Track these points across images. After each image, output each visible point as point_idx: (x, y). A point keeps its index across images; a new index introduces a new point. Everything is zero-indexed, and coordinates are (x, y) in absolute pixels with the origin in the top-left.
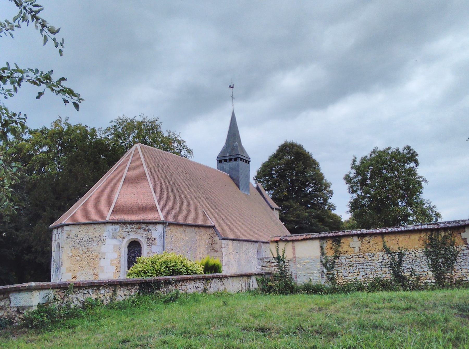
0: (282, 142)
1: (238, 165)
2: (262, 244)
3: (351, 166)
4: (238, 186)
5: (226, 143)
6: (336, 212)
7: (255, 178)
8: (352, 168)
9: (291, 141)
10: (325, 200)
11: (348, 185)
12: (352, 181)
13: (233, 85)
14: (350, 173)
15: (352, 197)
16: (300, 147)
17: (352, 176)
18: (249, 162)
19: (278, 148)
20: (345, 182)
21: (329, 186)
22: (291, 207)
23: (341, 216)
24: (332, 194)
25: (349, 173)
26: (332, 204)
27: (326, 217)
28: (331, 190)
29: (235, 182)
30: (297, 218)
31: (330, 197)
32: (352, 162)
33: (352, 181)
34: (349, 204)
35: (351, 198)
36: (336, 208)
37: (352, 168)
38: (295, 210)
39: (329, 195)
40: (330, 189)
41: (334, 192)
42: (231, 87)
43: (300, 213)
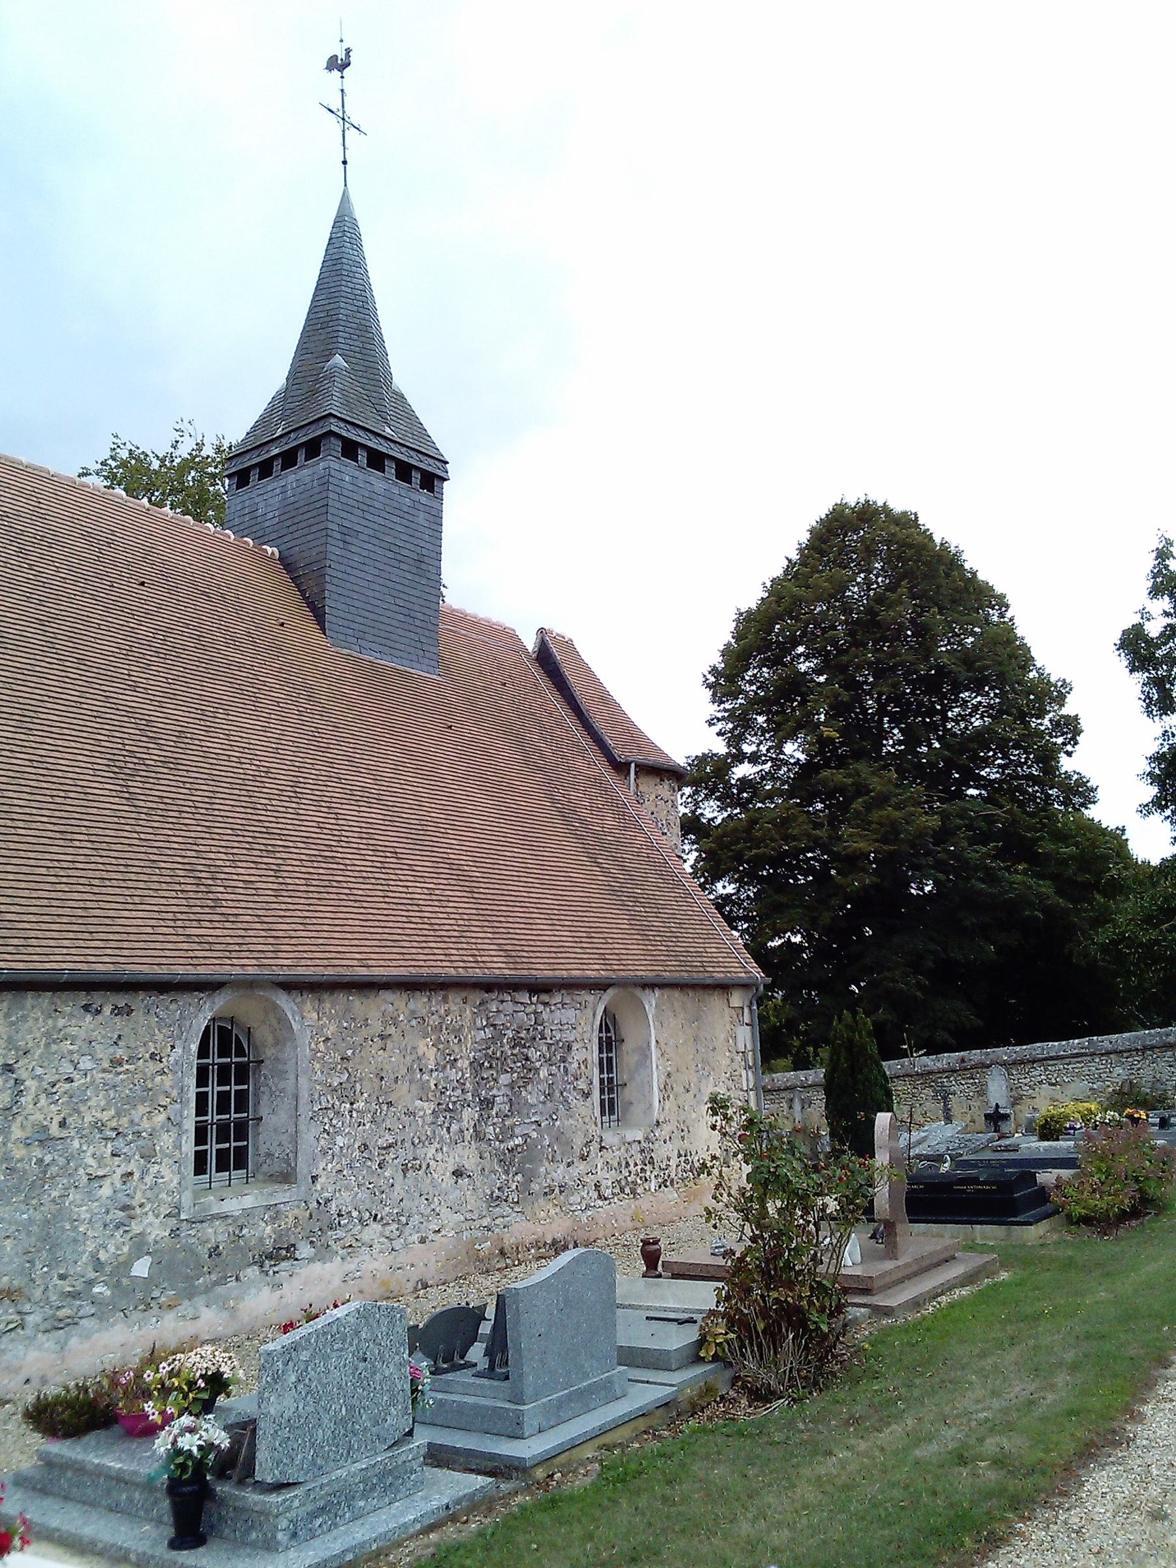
0: (821, 510)
1: (325, 482)
2: (283, 1001)
3: (1150, 584)
4: (319, 617)
5: (294, 376)
6: (1103, 813)
7: (712, 679)
8: (1156, 592)
9: (862, 501)
10: (1048, 758)
11: (1141, 676)
12: (1159, 653)
13: (348, 51)
14: (1146, 615)
15: (1161, 731)
16: (908, 521)
17: (1154, 629)
18: (432, 481)
19: (805, 537)
20: (1121, 663)
21: (1061, 700)
22: (861, 789)
23: (1123, 830)
24: (1077, 732)
25: (1137, 619)
26: (1075, 777)
27: (1042, 838)
28: (1072, 714)
29: (303, 592)
30: (884, 840)
31: (1069, 748)
32: (1150, 562)
33: (1159, 653)
34: (1148, 769)
35: (1161, 741)
36: (1100, 794)
37: (1156, 592)
38: (882, 800)
39: (1060, 740)
40: (1068, 710)
41: (1084, 723)
42: (338, 65)
43: (897, 814)
